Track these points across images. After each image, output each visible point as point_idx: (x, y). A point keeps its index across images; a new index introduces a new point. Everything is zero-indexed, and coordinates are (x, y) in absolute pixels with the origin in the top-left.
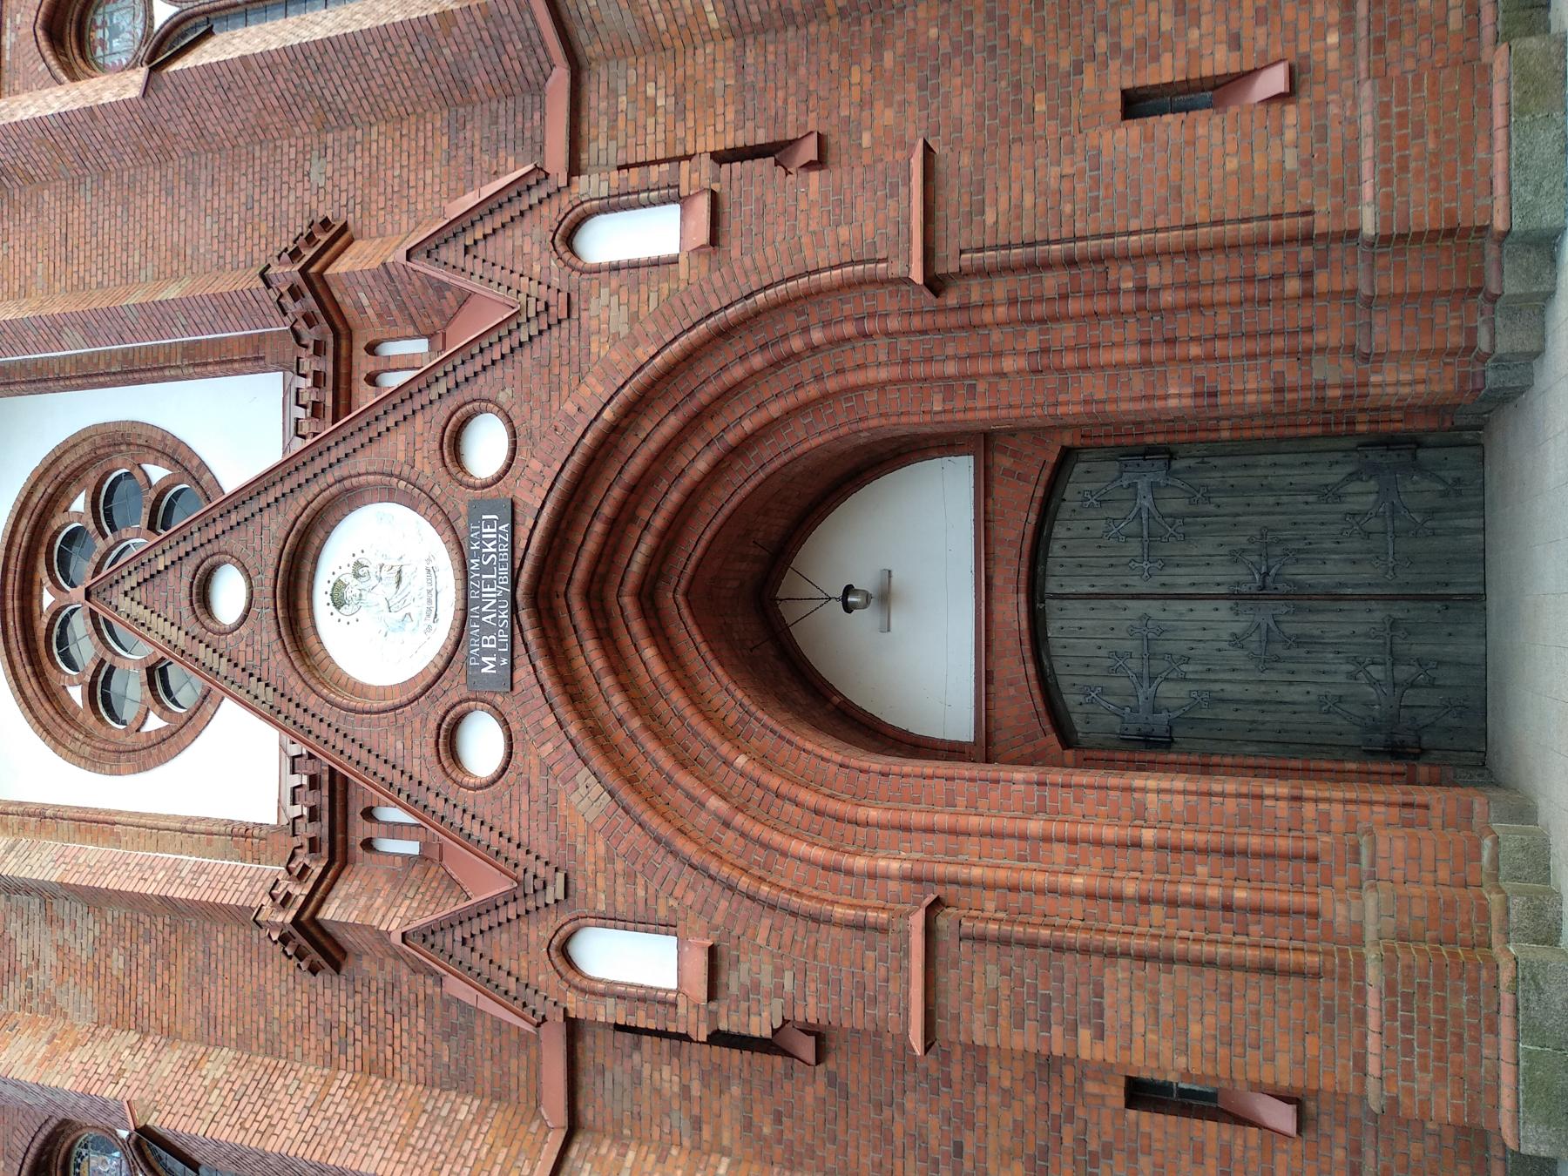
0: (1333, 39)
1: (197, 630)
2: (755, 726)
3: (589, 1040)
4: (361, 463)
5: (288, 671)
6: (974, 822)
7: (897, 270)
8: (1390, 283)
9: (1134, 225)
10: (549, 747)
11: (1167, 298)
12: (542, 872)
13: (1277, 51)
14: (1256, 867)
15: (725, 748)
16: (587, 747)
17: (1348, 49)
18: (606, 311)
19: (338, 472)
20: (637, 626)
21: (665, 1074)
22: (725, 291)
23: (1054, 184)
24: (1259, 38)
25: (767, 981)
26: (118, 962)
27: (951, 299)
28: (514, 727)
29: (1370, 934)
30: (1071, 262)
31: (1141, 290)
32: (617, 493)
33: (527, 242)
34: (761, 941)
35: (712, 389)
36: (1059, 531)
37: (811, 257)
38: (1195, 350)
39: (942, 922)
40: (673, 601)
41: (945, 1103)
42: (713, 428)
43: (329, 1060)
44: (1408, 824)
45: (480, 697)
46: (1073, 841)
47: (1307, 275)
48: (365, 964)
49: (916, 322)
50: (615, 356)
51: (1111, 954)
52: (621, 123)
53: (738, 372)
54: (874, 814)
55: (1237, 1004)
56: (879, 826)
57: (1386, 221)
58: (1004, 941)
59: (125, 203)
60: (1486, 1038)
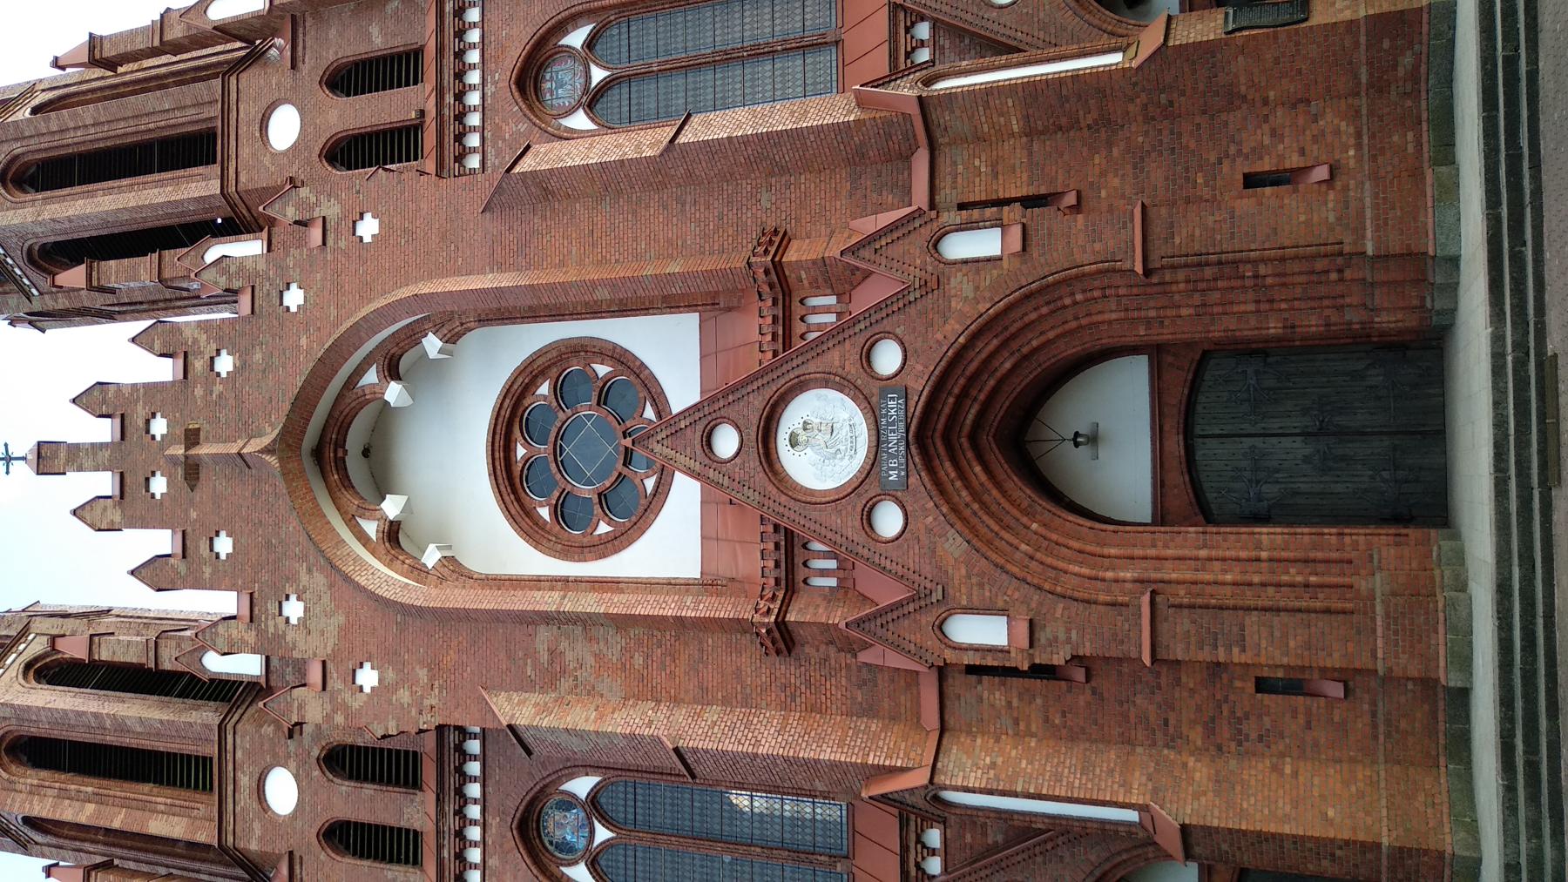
0: (1352, 153)
1: (707, 461)
2: (1039, 509)
3: (950, 680)
4: (811, 367)
5: (767, 483)
6: (1169, 552)
7: (1127, 265)
8: (1381, 276)
9: (1253, 247)
10: (930, 519)
11: (1269, 281)
12: (929, 585)
13: (1324, 158)
14: (1321, 568)
15: (1024, 520)
16: (952, 518)
17: (1359, 158)
18: (960, 284)
19: (797, 372)
20: (970, 455)
21: (994, 694)
22: (1029, 276)
23: (1211, 224)
24: (1314, 150)
25: (1062, 636)
26: (638, 660)
27: (1155, 280)
28: (909, 508)
29: (1378, 594)
30: (1220, 263)
31: (1256, 277)
32: (962, 381)
33: (913, 247)
34: (1058, 615)
35: (1018, 325)
36: (1202, 398)
37: (1079, 258)
38: (1284, 306)
39: (1159, 599)
40: (987, 440)
41: (1158, 698)
42: (1014, 345)
43: (784, 707)
44: (1397, 544)
45: (888, 494)
46: (1224, 560)
47: (1340, 271)
48: (807, 649)
49: (1135, 291)
50: (967, 309)
51: (1248, 609)
52: (959, 180)
53: (1033, 316)
54: (1113, 551)
55: (1313, 629)
56: (1118, 557)
57: (1377, 248)
58: (1192, 607)
59: (634, 213)
60: (1433, 635)
